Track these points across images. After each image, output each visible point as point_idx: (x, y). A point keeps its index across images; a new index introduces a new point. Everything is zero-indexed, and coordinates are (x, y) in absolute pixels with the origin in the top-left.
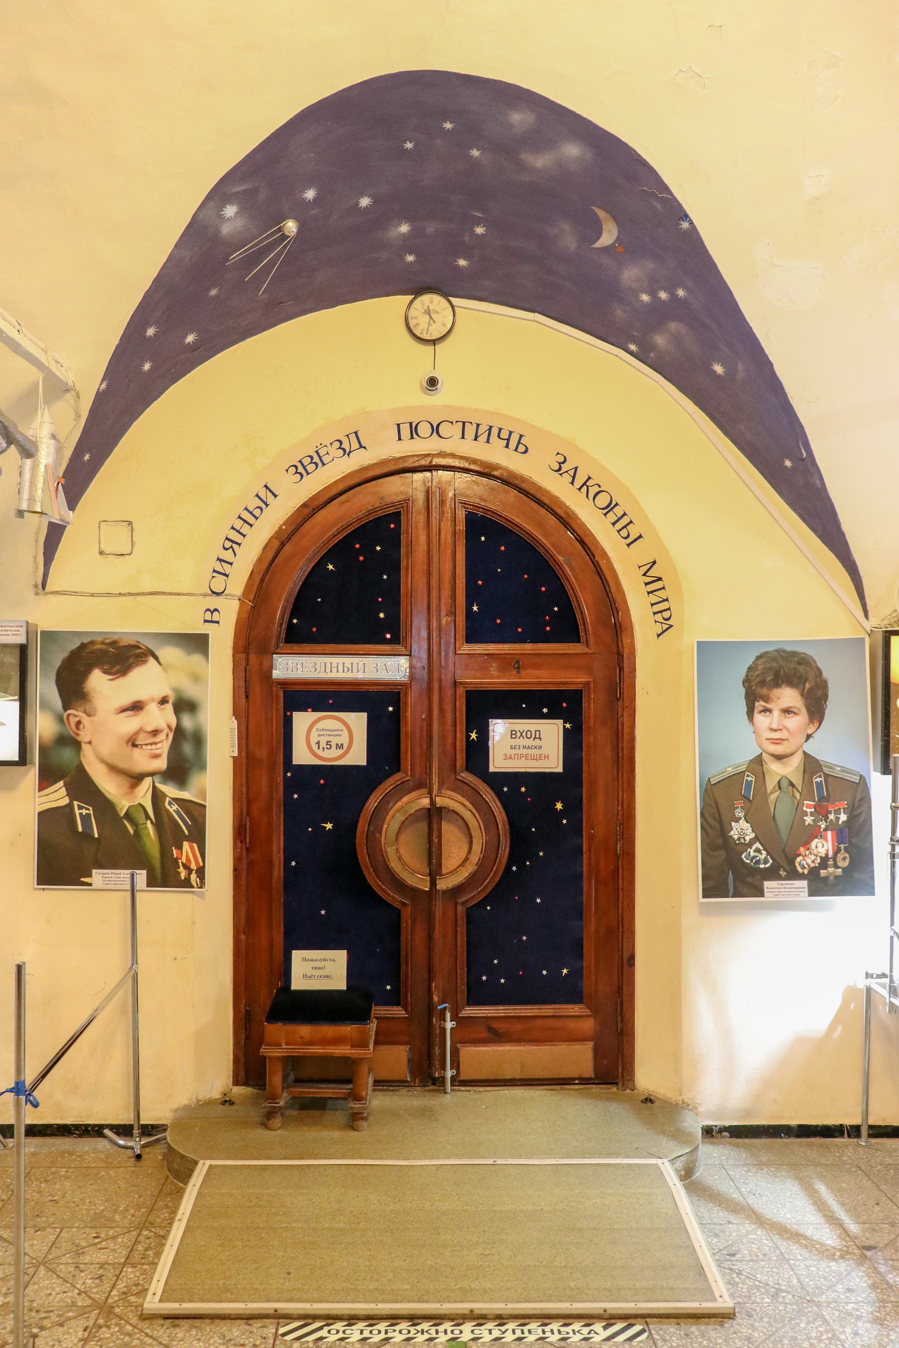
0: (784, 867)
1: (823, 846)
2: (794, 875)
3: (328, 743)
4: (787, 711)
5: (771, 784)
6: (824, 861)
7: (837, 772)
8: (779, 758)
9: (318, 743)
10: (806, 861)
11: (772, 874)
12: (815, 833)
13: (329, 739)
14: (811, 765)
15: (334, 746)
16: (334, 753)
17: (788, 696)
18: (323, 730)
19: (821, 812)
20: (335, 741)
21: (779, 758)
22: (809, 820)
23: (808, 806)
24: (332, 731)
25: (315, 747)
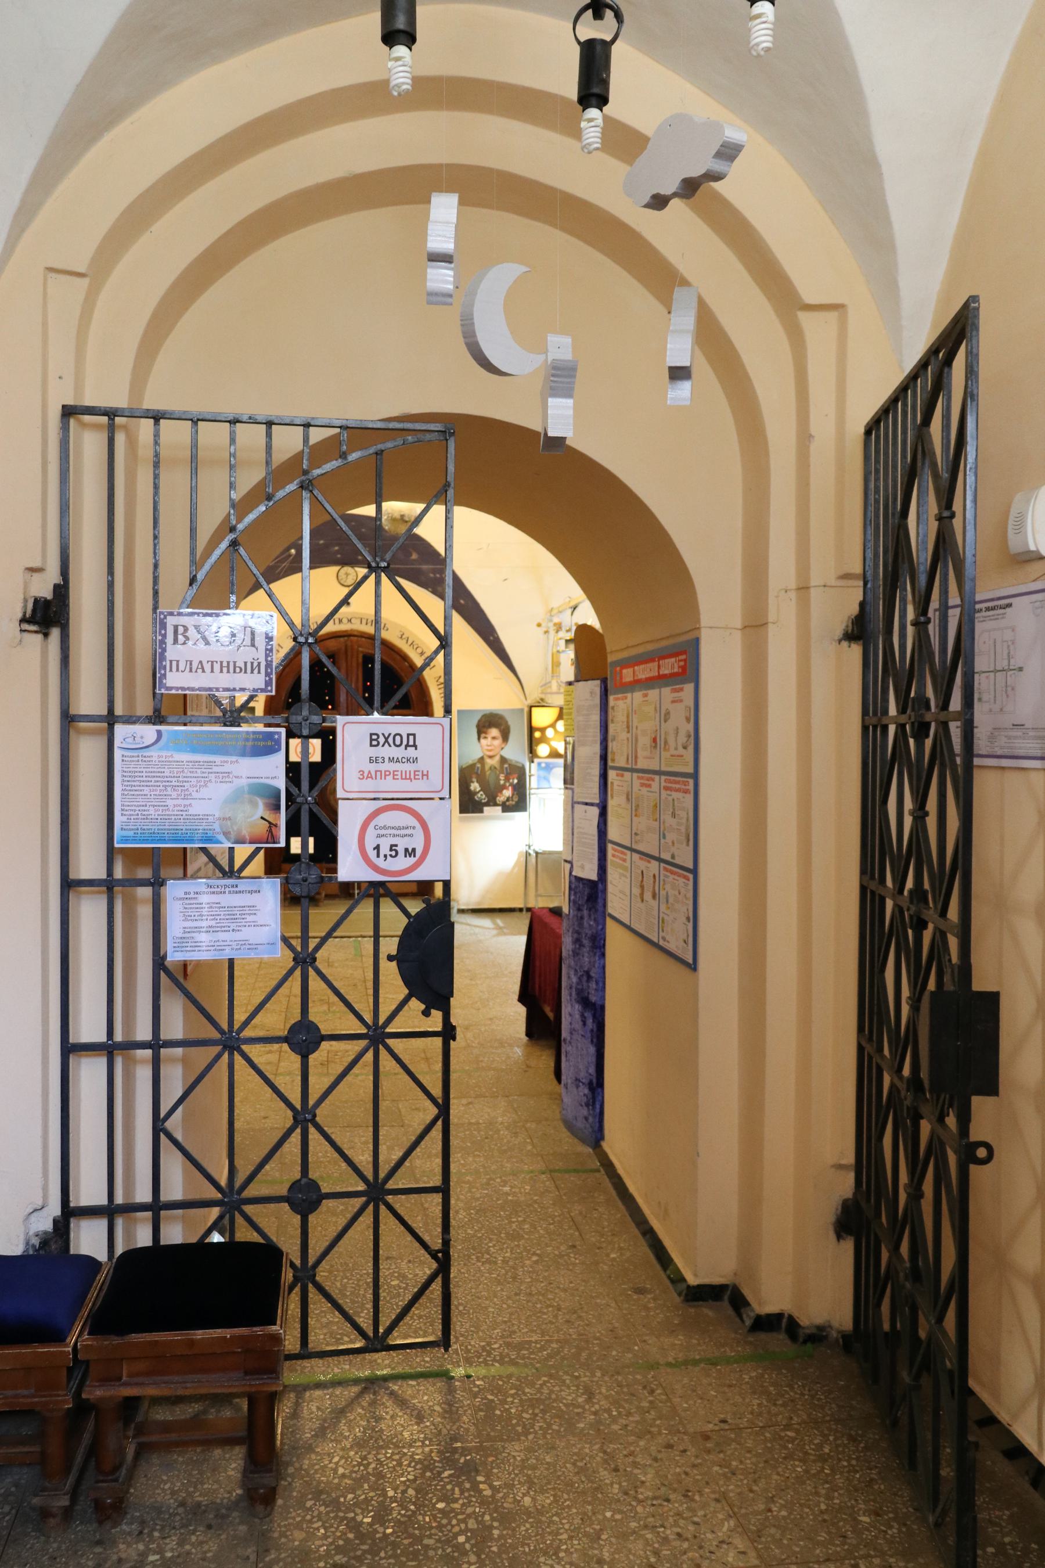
0: (492, 802)
1: (507, 793)
2: (496, 804)
3: (392, 847)
4: (494, 738)
5: (487, 767)
6: (508, 800)
7: (513, 763)
8: (491, 757)
9: (377, 848)
10: (500, 799)
11: (487, 804)
12: (504, 787)
13: (394, 841)
14: (503, 760)
15: (401, 853)
16: (402, 863)
17: (494, 732)
18: (381, 828)
19: (507, 779)
20: (402, 844)
21: (491, 757)
22: (502, 782)
23: (502, 777)
24: (399, 828)
25: (372, 854)
